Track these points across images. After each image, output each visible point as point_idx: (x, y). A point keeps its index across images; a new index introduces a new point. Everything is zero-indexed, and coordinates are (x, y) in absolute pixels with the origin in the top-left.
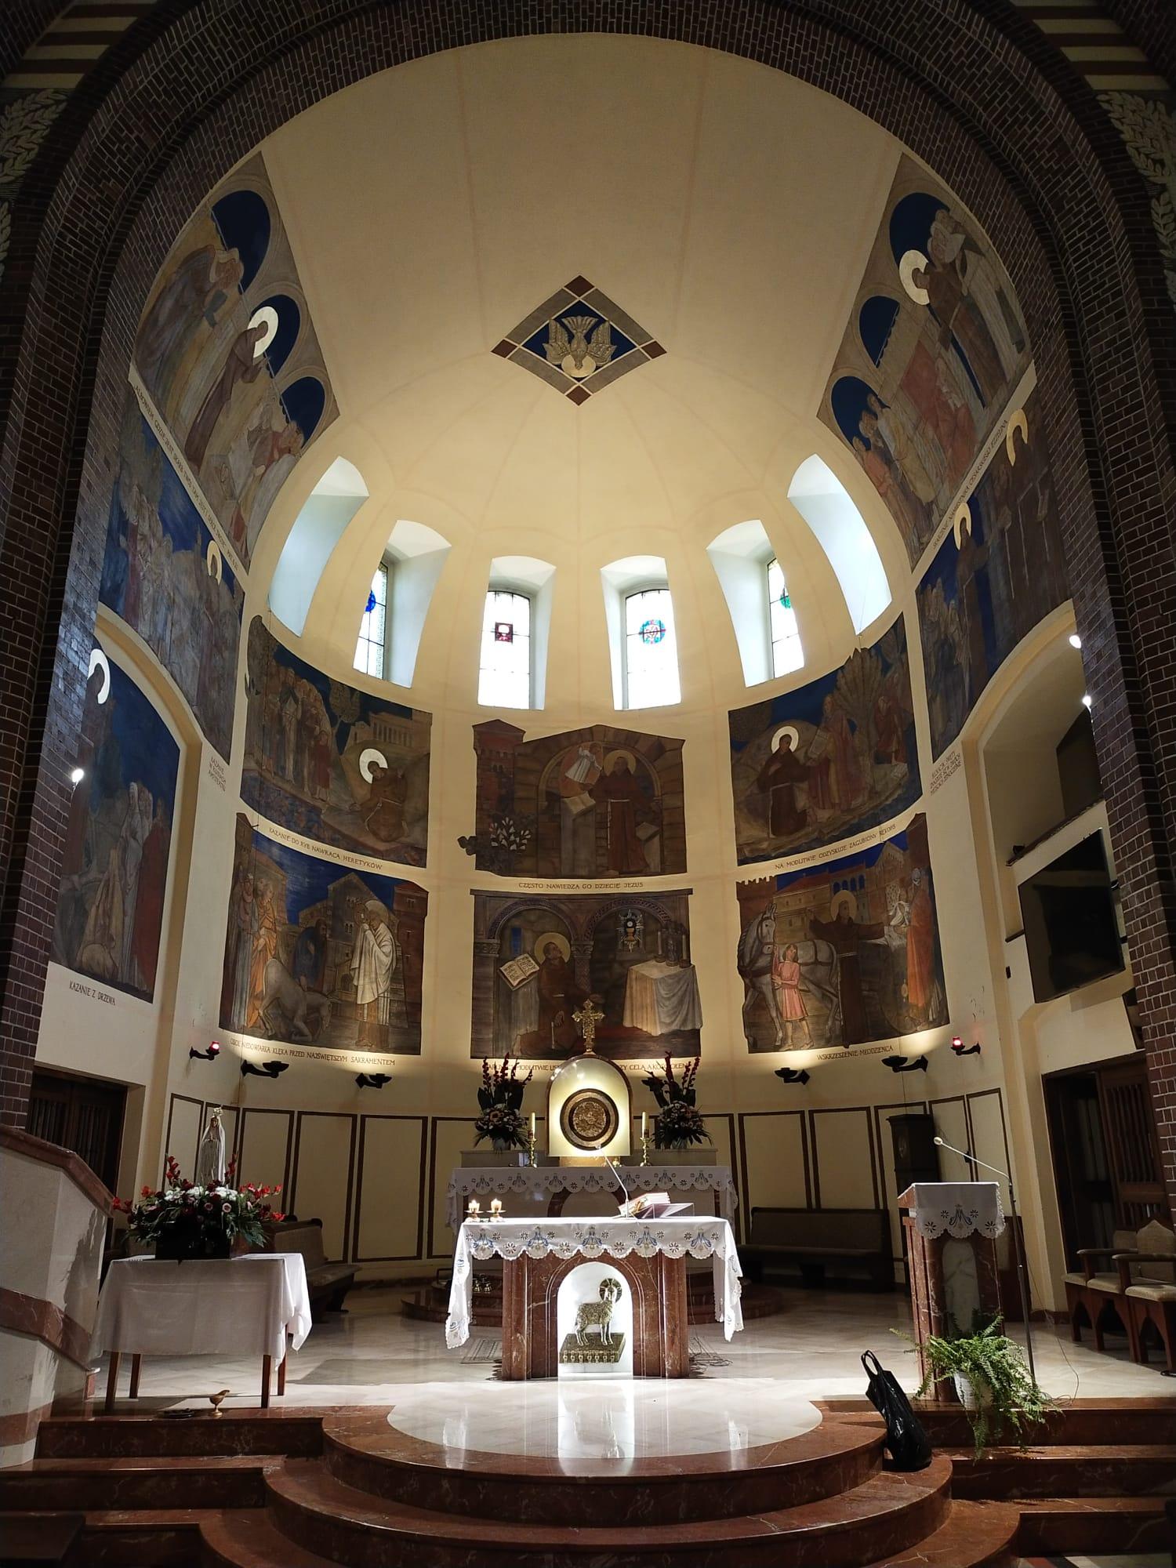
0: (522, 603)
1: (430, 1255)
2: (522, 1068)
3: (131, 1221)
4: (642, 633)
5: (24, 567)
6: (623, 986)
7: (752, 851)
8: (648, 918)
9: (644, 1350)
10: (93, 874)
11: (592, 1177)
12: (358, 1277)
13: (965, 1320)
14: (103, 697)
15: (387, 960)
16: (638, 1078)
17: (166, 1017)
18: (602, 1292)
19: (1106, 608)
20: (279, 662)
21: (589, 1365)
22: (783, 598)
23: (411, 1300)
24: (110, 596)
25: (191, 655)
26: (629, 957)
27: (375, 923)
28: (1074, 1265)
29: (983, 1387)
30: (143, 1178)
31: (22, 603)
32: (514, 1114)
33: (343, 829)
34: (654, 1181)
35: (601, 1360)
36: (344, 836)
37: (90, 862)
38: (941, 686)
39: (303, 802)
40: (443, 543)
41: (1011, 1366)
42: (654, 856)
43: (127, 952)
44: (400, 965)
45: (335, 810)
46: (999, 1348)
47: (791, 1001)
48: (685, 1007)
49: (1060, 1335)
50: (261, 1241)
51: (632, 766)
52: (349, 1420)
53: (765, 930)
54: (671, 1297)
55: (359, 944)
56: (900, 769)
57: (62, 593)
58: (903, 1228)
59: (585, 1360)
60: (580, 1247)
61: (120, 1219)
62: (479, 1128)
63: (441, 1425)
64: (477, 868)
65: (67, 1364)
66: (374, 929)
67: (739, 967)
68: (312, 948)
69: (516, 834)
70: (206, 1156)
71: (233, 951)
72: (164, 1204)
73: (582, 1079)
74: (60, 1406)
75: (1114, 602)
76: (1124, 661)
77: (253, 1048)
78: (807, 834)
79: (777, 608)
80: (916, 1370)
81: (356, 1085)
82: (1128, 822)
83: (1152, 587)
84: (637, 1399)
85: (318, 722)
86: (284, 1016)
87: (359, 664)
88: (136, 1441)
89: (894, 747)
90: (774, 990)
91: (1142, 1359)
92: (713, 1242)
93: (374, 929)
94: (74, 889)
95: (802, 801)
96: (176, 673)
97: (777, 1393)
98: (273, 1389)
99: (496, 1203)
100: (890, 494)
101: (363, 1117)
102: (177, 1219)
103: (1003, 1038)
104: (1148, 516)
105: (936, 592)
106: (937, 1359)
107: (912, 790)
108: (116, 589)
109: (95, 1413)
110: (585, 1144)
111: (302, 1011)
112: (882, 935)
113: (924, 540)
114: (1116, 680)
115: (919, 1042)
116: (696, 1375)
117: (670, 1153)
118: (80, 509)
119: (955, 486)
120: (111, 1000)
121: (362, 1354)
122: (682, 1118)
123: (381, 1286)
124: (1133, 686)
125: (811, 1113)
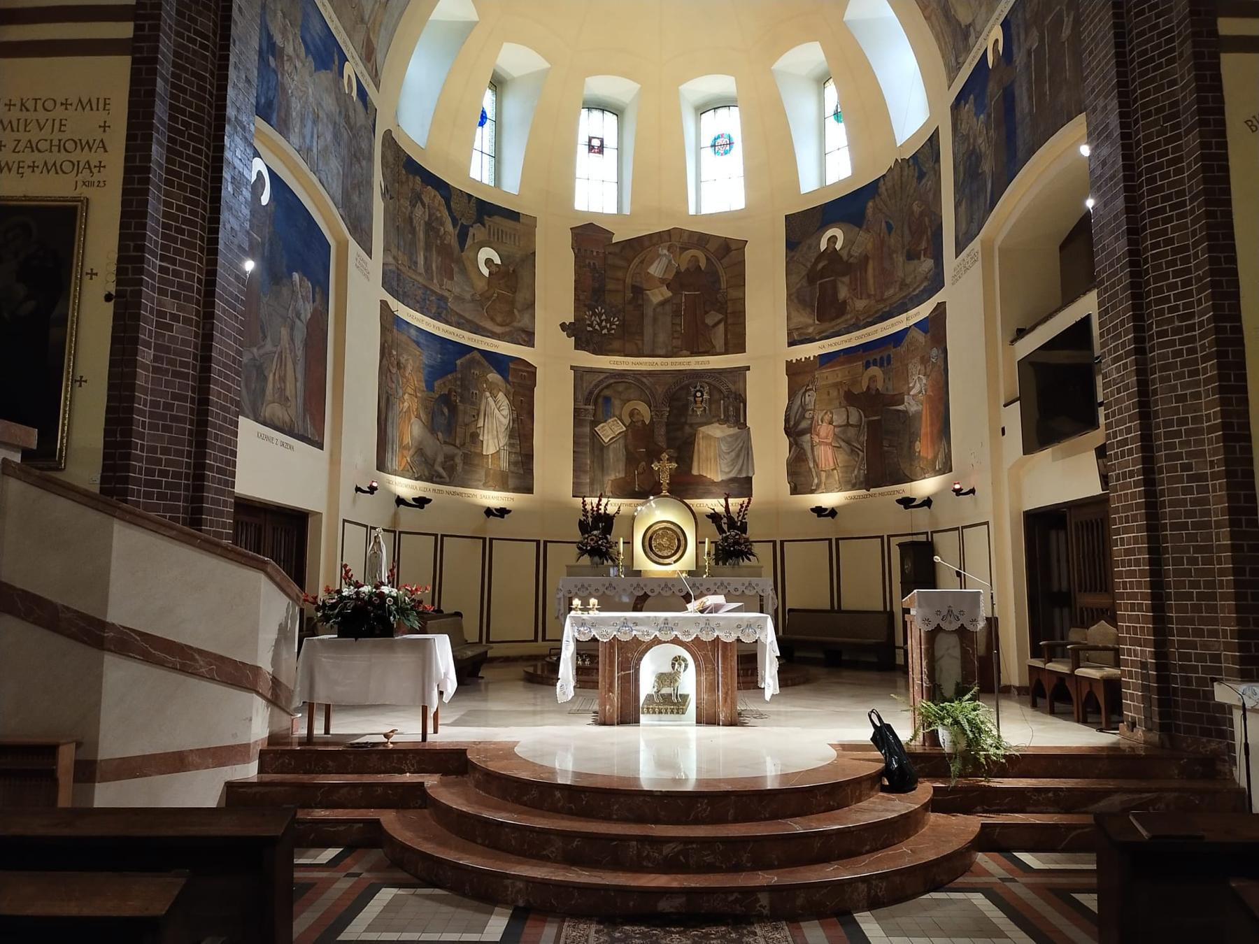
0: (611, 119)
1: (544, 639)
2: (612, 505)
3: (317, 610)
4: (714, 146)
5: (191, 84)
6: (693, 443)
7: (800, 335)
8: (713, 389)
9: (704, 705)
10: (269, 347)
11: (666, 585)
12: (490, 654)
13: (949, 689)
14: (265, 199)
15: (506, 421)
17: (335, 461)
18: (673, 665)
19: (1114, 121)
20: (410, 174)
21: (663, 716)
22: (836, 114)
23: (531, 670)
24: (264, 111)
25: (335, 164)
26: (699, 420)
28: (1036, 652)
29: (960, 737)
30: (325, 579)
31: (192, 116)
33: (467, 315)
34: (713, 588)
35: (672, 712)
36: (468, 321)
37: (265, 337)
38: (967, 191)
39: (433, 292)
40: (547, 65)
41: (982, 722)
43: (301, 410)
45: (459, 298)
46: (974, 710)
47: (825, 455)
49: (1022, 703)
50: (417, 625)
51: (703, 264)
52: (486, 750)
54: (727, 671)
55: (482, 408)
56: (927, 264)
57: (224, 107)
58: (905, 623)
59: (660, 712)
60: (657, 633)
61: (310, 610)
62: (579, 548)
63: (554, 754)
65: (277, 710)
66: (494, 397)
68: (446, 411)
69: (607, 321)
70: (372, 564)
71: (383, 410)
72: (342, 598)
73: (658, 513)
74: (273, 739)
75: (1121, 115)
76: (1125, 168)
77: (405, 487)
79: (831, 122)
80: (910, 724)
82: (1114, 307)
83: (1156, 101)
84: (699, 739)
85: (442, 224)
86: (426, 462)
87: (475, 173)
88: (330, 763)
89: (923, 245)
90: (812, 447)
91: (1083, 720)
92: (758, 631)
93: (494, 397)
94: (254, 359)
95: (843, 293)
96: (324, 180)
97: (804, 738)
98: (430, 729)
99: (593, 601)
100: (933, 18)
101: (491, 540)
102: (353, 609)
103: (994, 480)
104: (1160, 35)
105: (968, 108)
106: (925, 717)
107: (937, 282)
108: (270, 104)
109: (300, 744)
110: (661, 561)
111: (440, 459)
113: (961, 60)
114: (1116, 185)
115: (926, 486)
116: (743, 724)
117: (727, 568)
118: (234, 31)
119: (991, 10)
120: (291, 448)
121: (494, 706)
122: (737, 543)
123: (508, 660)
124: (1131, 192)
125: (837, 540)
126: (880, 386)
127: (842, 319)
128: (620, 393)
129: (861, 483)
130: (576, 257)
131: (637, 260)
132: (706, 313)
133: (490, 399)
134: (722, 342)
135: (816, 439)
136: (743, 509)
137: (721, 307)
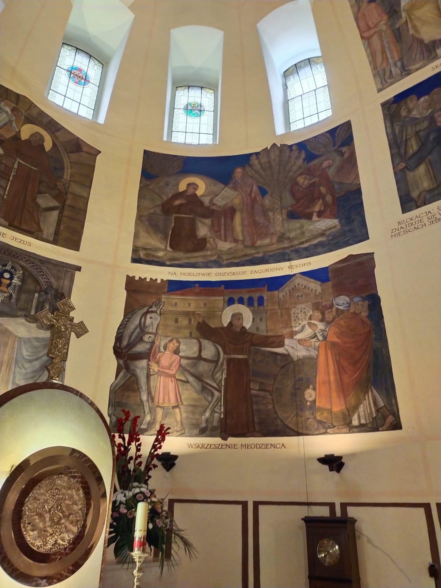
7: (147, 255)
51: (48, 145)
53: (148, 321)
67: (114, 348)
78: (205, 256)
90: (148, 376)
95: (203, 231)
112: (281, 344)
129: (214, 429)
132: (40, 192)
134: (52, 230)
135: (154, 367)
137: (60, 196)
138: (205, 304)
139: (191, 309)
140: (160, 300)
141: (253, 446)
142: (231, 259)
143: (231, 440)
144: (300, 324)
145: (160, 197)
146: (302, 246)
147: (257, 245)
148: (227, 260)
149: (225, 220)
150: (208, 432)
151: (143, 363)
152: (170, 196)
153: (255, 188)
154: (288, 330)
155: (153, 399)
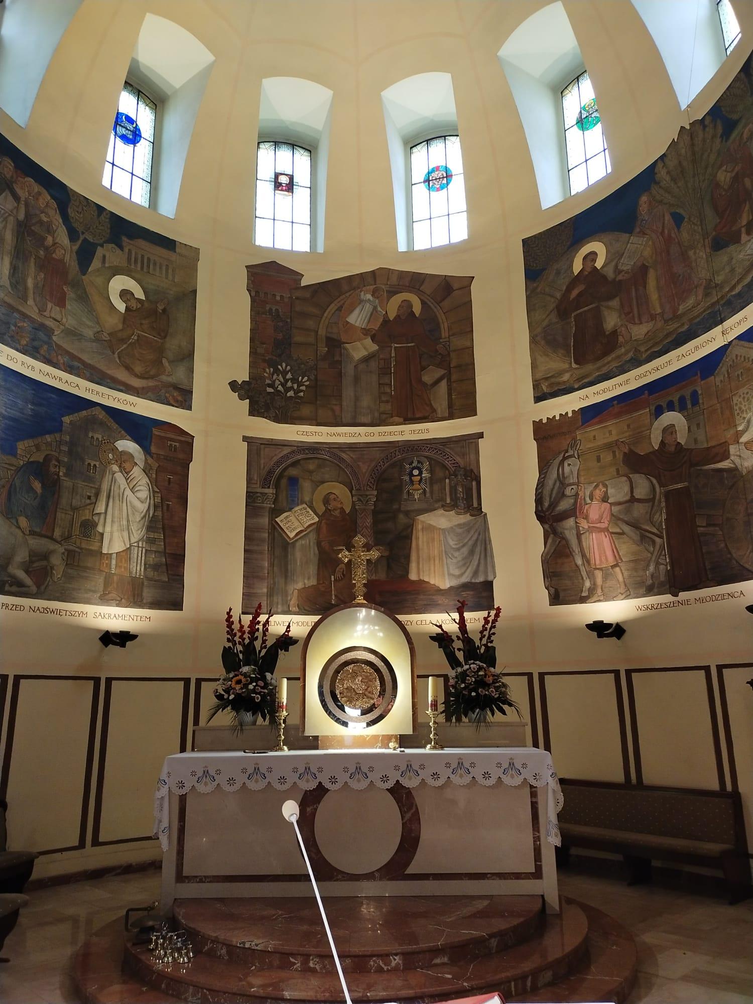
4: (427, 181)
7: (551, 385)
8: (434, 465)
11: (358, 769)
15: (142, 507)
16: (422, 635)
26: (416, 506)
27: (127, 465)
32: (264, 678)
33: (85, 357)
36: (87, 366)
42: (441, 403)
44: (159, 513)
45: (71, 333)
47: (599, 544)
48: (476, 557)
51: (417, 309)
53: (567, 469)
55: (105, 487)
64: (251, 413)
66: (126, 472)
68: (37, 486)
69: (294, 380)
73: (363, 632)
78: (619, 357)
79: (574, 135)
81: (100, 643)
85: (49, 230)
90: (579, 536)
93: (126, 472)
95: (611, 320)
101: (109, 681)
111: (22, 556)
112: (726, 456)
122: (481, 683)
125: (629, 672)
126: (682, 438)
127: (613, 355)
128: (311, 472)
129: (662, 584)
130: (253, 300)
131: (333, 307)
132: (423, 369)
133: (119, 476)
134: (445, 403)
135: (584, 524)
136: (489, 626)
137: (443, 361)
138: (628, 426)
139: (614, 438)
140: (575, 439)
141: (708, 599)
142: (651, 347)
143: (683, 595)
144: (744, 418)
145: (552, 296)
146: (734, 293)
147: (679, 312)
148: (646, 351)
149: (636, 290)
150: (656, 590)
151: (571, 522)
152: (565, 288)
153: (668, 217)
154: (732, 432)
155: (588, 562)
